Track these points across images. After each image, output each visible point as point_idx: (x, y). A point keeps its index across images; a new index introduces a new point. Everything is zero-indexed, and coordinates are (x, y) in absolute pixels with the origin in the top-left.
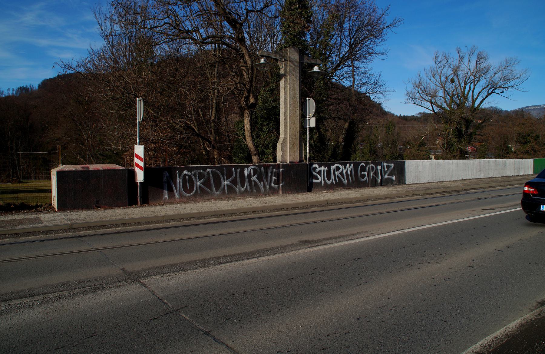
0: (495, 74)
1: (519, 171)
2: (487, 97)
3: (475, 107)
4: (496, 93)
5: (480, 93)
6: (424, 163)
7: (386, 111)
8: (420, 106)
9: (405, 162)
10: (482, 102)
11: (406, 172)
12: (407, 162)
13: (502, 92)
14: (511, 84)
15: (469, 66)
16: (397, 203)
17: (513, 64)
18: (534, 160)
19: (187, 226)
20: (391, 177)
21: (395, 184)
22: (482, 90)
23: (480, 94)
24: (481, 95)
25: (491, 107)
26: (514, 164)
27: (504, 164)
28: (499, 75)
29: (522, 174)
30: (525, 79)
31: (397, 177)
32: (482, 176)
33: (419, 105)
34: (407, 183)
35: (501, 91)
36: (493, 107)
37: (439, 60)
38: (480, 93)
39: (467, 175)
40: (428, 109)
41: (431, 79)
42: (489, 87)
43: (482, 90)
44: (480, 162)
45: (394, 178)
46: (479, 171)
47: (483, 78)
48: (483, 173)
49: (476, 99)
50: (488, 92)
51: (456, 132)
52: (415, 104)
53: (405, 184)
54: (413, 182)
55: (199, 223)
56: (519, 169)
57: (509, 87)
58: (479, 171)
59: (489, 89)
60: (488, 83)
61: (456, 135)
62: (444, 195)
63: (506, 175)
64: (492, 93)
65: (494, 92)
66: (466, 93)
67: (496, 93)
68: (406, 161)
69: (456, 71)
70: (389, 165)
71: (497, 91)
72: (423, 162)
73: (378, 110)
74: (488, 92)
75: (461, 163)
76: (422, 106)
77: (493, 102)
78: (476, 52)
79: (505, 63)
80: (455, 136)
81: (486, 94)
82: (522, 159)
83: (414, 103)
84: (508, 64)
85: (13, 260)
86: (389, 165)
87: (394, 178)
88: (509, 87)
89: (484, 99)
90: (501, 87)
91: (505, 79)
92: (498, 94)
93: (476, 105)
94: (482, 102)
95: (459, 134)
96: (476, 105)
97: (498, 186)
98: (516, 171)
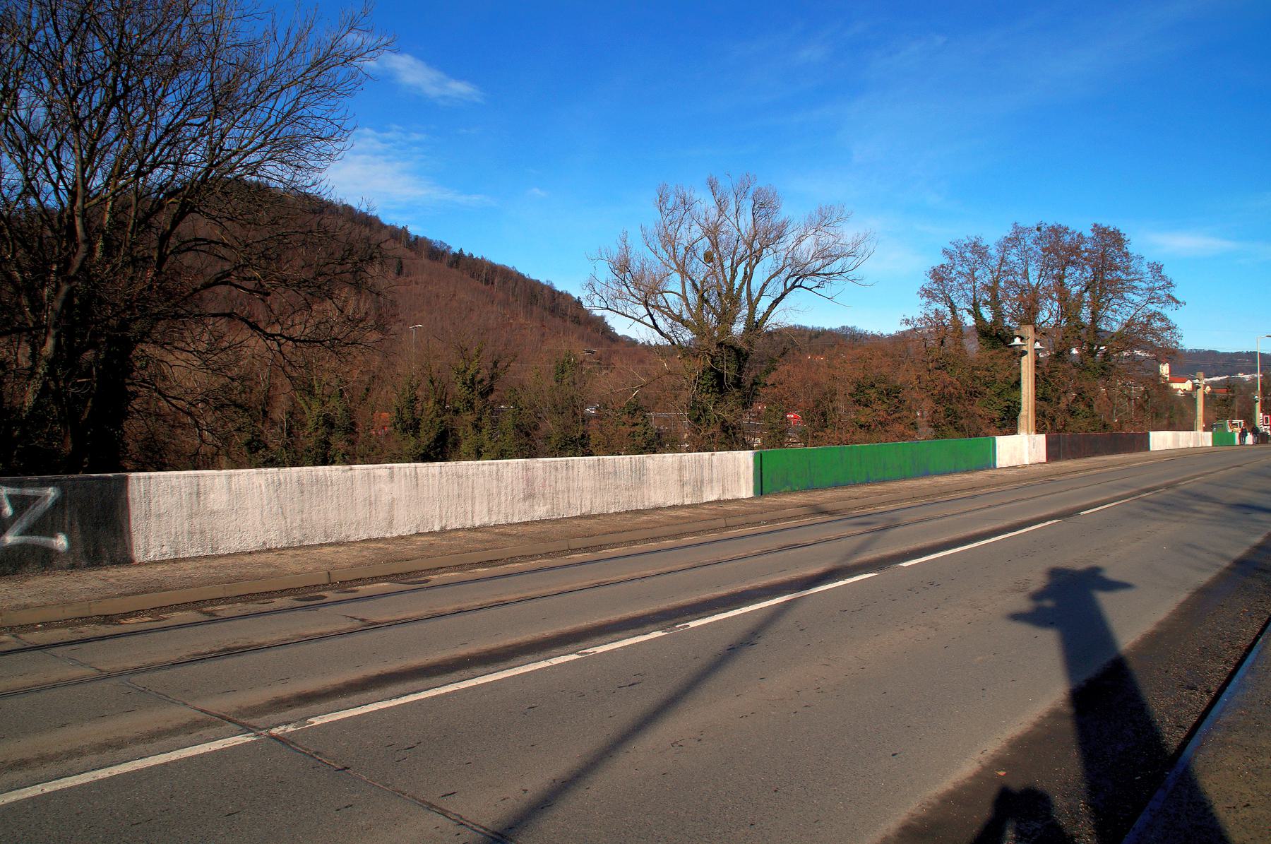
0: (799, 241)
1: (702, 491)
2: (783, 296)
3: (756, 319)
4: (806, 288)
5: (765, 285)
6: (235, 479)
7: (616, 334)
8: (624, 315)
9: (126, 478)
10: (772, 307)
11: (132, 518)
12: (139, 479)
13: (818, 287)
14: (836, 266)
15: (738, 221)
16: (530, 575)
17: (835, 219)
18: (755, 455)
19: (516, 574)
20: (48, 539)
21: (66, 564)
22: (769, 280)
23: (767, 287)
24: (768, 290)
25: (843, 327)
26: (680, 469)
27: (640, 472)
28: (808, 244)
29: (713, 498)
30: (864, 258)
31: (78, 536)
32: (540, 511)
33: (619, 313)
34: (138, 555)
35: (817, 284)
36: (847, 327)
37: (670, 205)
38: (765, 285)
39: (465, 513)
40: (639, 321)
41: (658, 252)
42: (788, 270)
43: (769, 280)
44: (527, 470)
45: (61, 542)
46: (524, 499)
47: (771, 251)
48: (545, 505)
49: (758, 299)
50: (785, 284)
51: (712, 379)
52: (610, 310)
53: (128, 561)
54: (176, 553)
55: (53, 642)
56: (699, 485)
57: (832, 274)
58: (524, 499)
59: (788, 278)
60: (781, 263)
61: (712, 386)
62: (354, 591)
63: (648, 504)
64: (793, 286)
65: (800, 286)
66: (736, 286)
67: (806, 288)
68: (133, 474)
69: (712, 232)
70: (29, 492)
71: (806, 283)
72: (230, 476)
73: (598, 332)
74: (785, 284)
75: (434, 476)
76: (627, 316)
77: (797, 308)
78: (751, 188)
79: (818, 219)
80: (711, 390)
81: (781, 289)
82: (710, 453)
83: (608, 308)
84: (826, 221)
85: (1023, 500)
86: (29, 492)
87: (61, 542)
88: (832, 274)
89: (776, 302)
90: (814, 274)
91: (827, 255)
92: (810, 290)
93: (758, 316)
94: (772, 307)
95: (718, 383)
96: (758, 316)
97: (902, 500)
98: (688, 489)
